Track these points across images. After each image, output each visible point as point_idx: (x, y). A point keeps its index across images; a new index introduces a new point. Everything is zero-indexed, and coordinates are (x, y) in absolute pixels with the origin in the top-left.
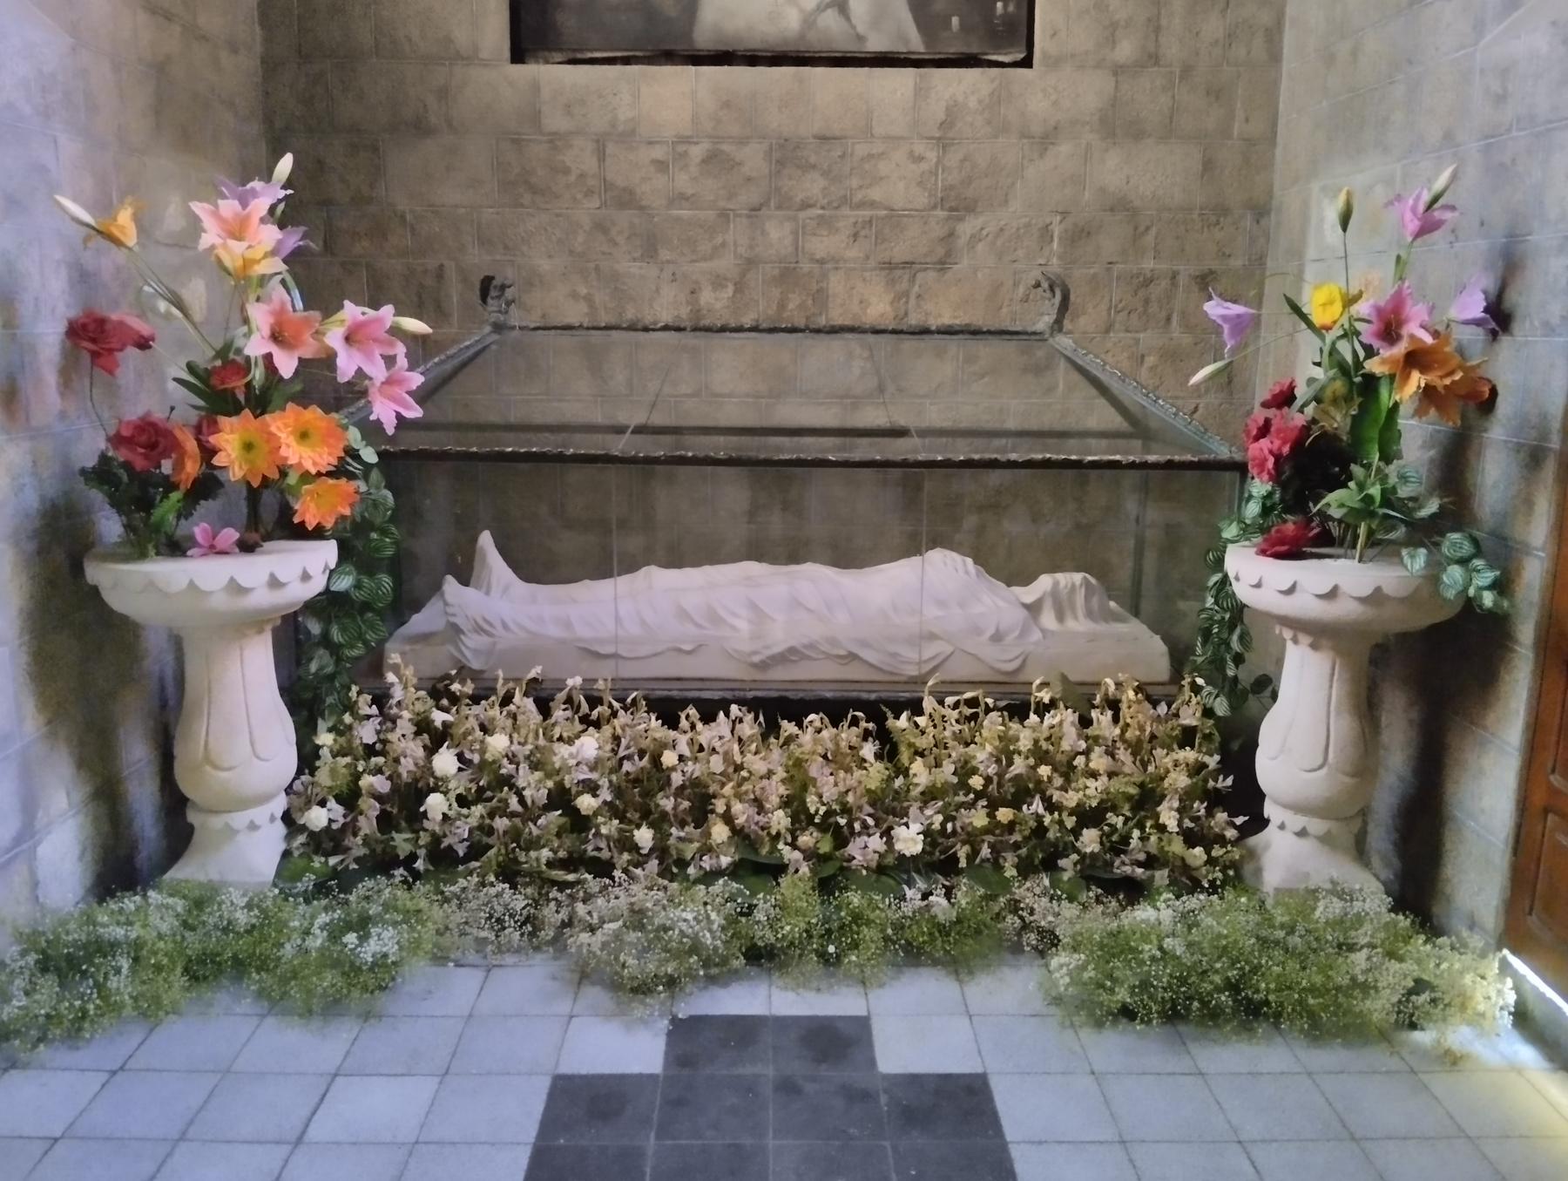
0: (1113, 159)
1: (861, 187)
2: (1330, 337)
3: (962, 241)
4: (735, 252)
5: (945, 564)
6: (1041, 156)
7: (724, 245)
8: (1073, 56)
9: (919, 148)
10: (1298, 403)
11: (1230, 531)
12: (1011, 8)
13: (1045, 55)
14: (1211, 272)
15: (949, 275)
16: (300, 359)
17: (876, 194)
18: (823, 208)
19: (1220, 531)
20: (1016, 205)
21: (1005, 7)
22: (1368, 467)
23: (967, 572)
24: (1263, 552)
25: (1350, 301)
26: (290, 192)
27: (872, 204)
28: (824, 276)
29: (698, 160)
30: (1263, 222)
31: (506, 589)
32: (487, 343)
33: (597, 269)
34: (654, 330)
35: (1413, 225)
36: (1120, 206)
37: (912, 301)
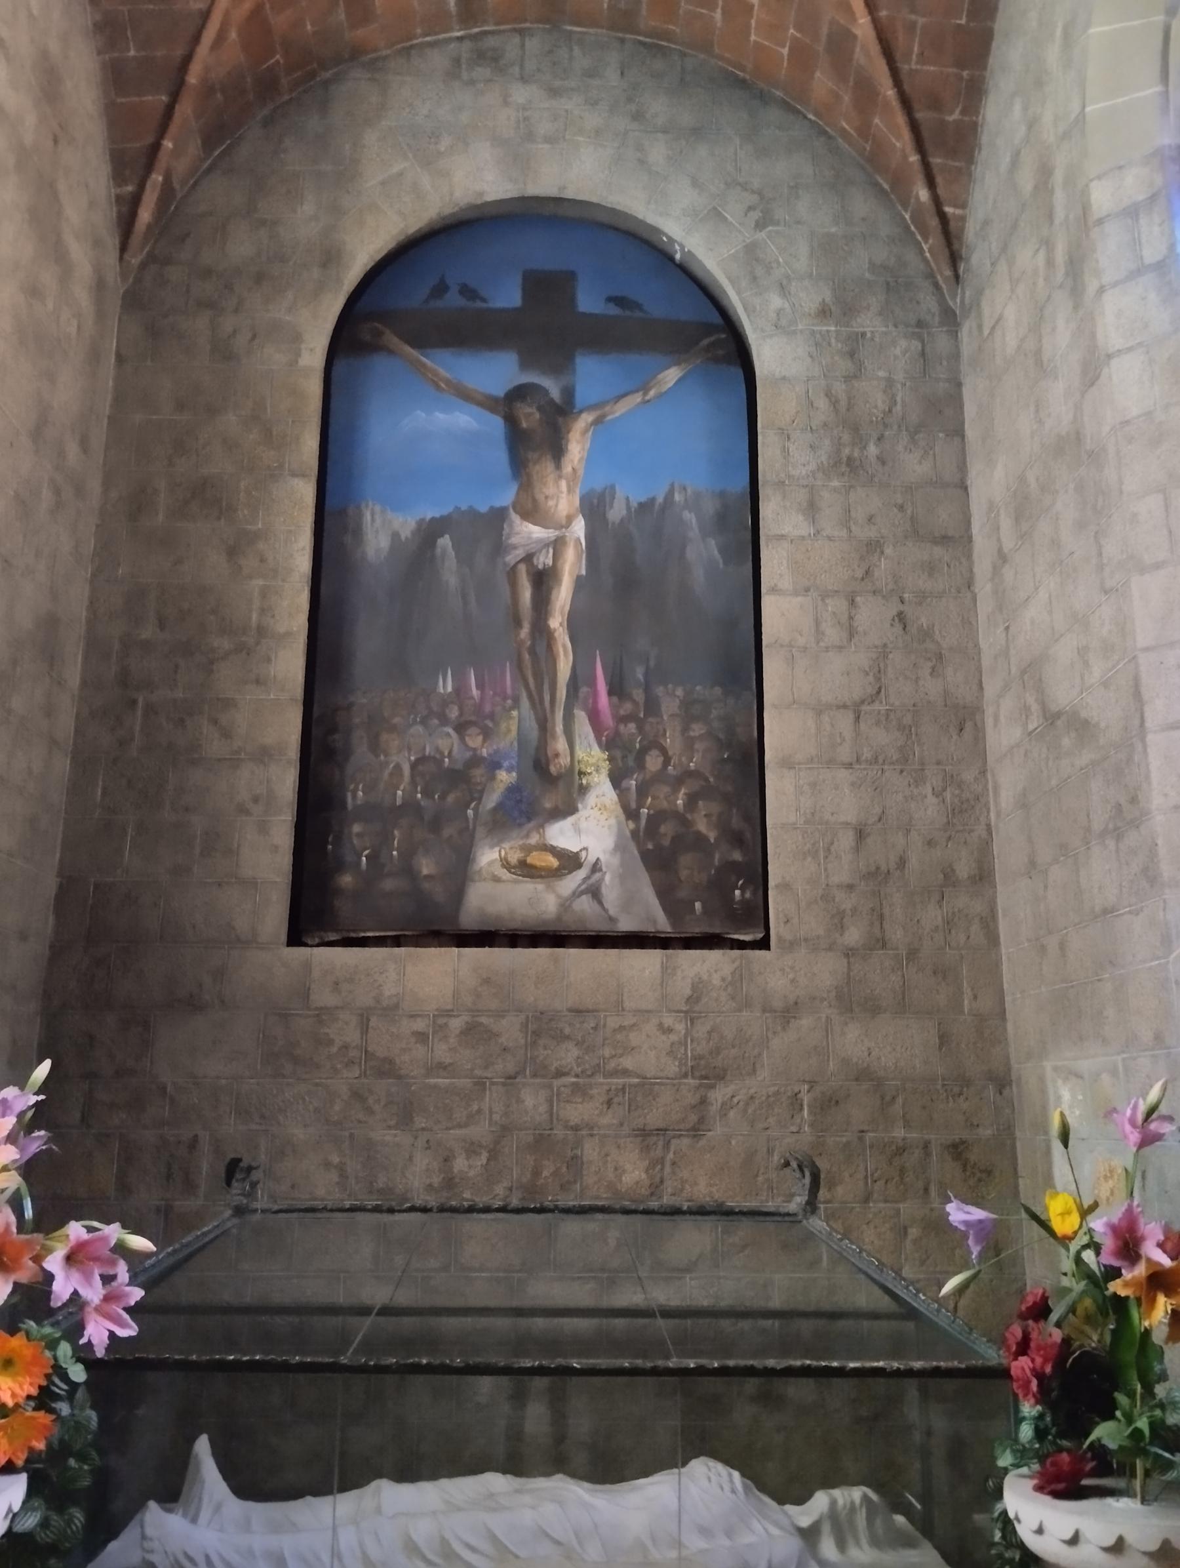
0: (853, 1032)
1: (613, 1057)
2: (1074, 1247)
3: (714, 1108)
4: (491, 1119)
5: (709, 1480)
6: (784, 1029)
7: (479, 1111)
8: (806, 940)
9: (668, 1021)
10: (1054, 1317)
11: (1005, 1460)
12: (748, 895)
13: (780, 939)
14: (963, 1142)
15: (703, 1142)
16: (16, 1284)
17: (628, 1062)
18: (577, 1076)
19: (994, 1459)
20: (764, 1074)
21: (743, 894)
22: (1131, 1395)
23: (733, 1491)
24: (1039, 1489)
25: (1085, 1212)
26: (42, 1097)
27: (625, 1072)
28: (578, 1143)
29: (457, 1032)
30: (1006, 1092)
31: (218, 1508)
32: (225, 1228)
33: (351, 1136)
34: (400, 1211)
35: (1134, 1137)
36: (863, 1074)
37: (668, 1169)
